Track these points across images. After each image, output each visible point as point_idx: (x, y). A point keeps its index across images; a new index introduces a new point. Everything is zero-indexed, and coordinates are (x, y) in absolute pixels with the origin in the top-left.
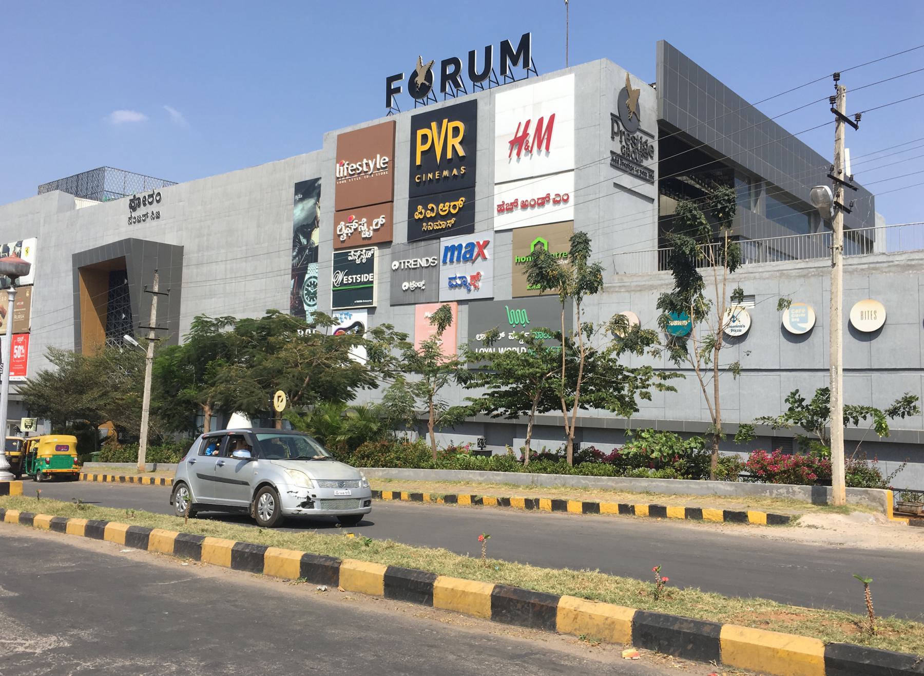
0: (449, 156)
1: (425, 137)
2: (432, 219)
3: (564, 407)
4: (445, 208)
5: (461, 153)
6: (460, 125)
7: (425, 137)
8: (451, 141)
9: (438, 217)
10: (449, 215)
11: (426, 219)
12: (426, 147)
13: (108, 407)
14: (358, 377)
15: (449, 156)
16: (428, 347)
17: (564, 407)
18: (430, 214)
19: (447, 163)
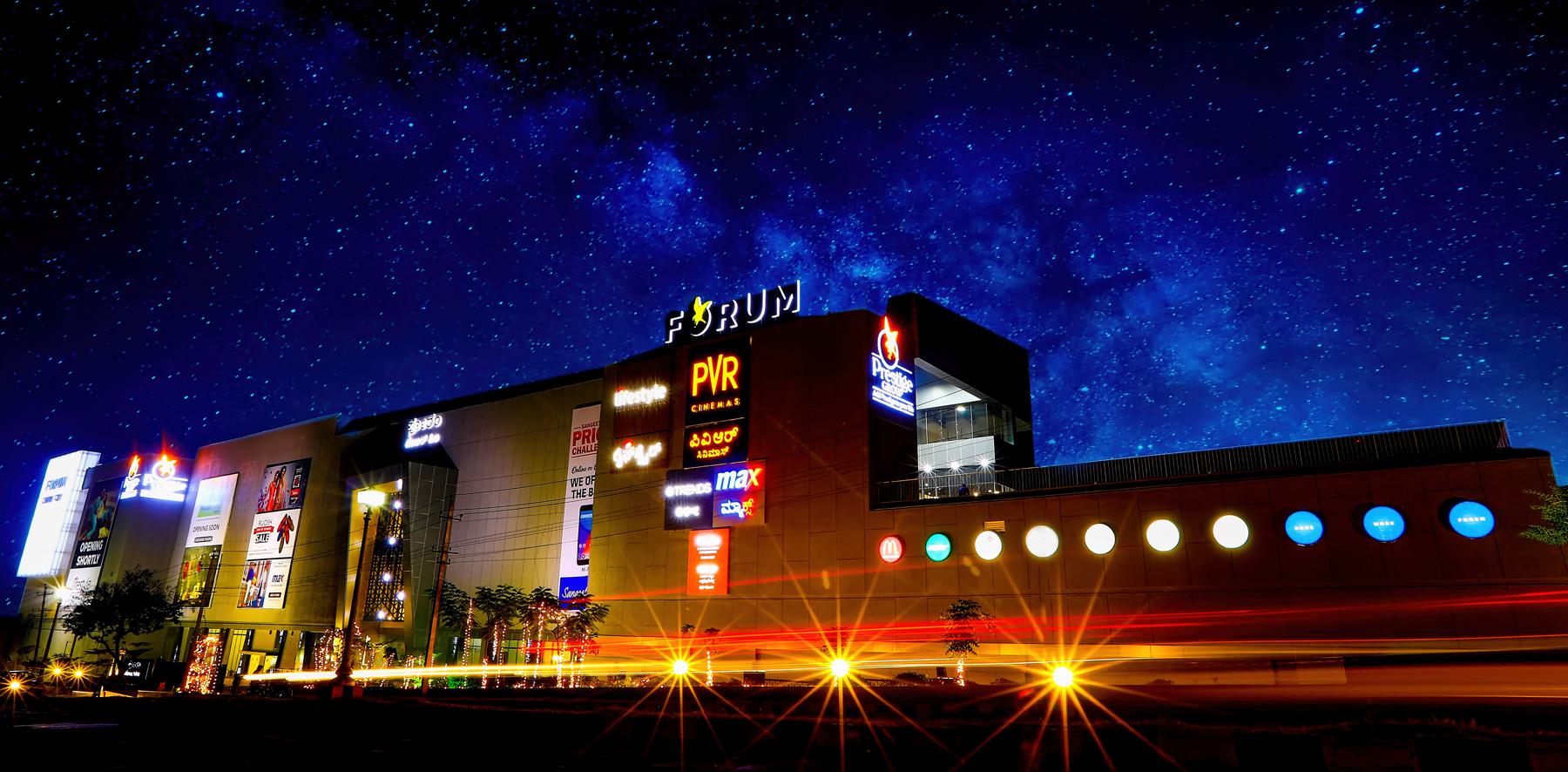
0: (724, 388)
1: (701, 372)
2: (708, 448)
3: (1040, 634)
4: (719, 437)
5: (735, 386)
6: (733, 359)
7: (701, 372)
8: (726, 374)
9: (713, 446)
10: (724, 444)
11: (701, 448)
12: (703, 380)
13: (728, 508)
14: (1230, 319)
15: (724, 388)
16: (1153, 288)
17: (1040, 634)
18: (704, 443)
19: (721, 395)
